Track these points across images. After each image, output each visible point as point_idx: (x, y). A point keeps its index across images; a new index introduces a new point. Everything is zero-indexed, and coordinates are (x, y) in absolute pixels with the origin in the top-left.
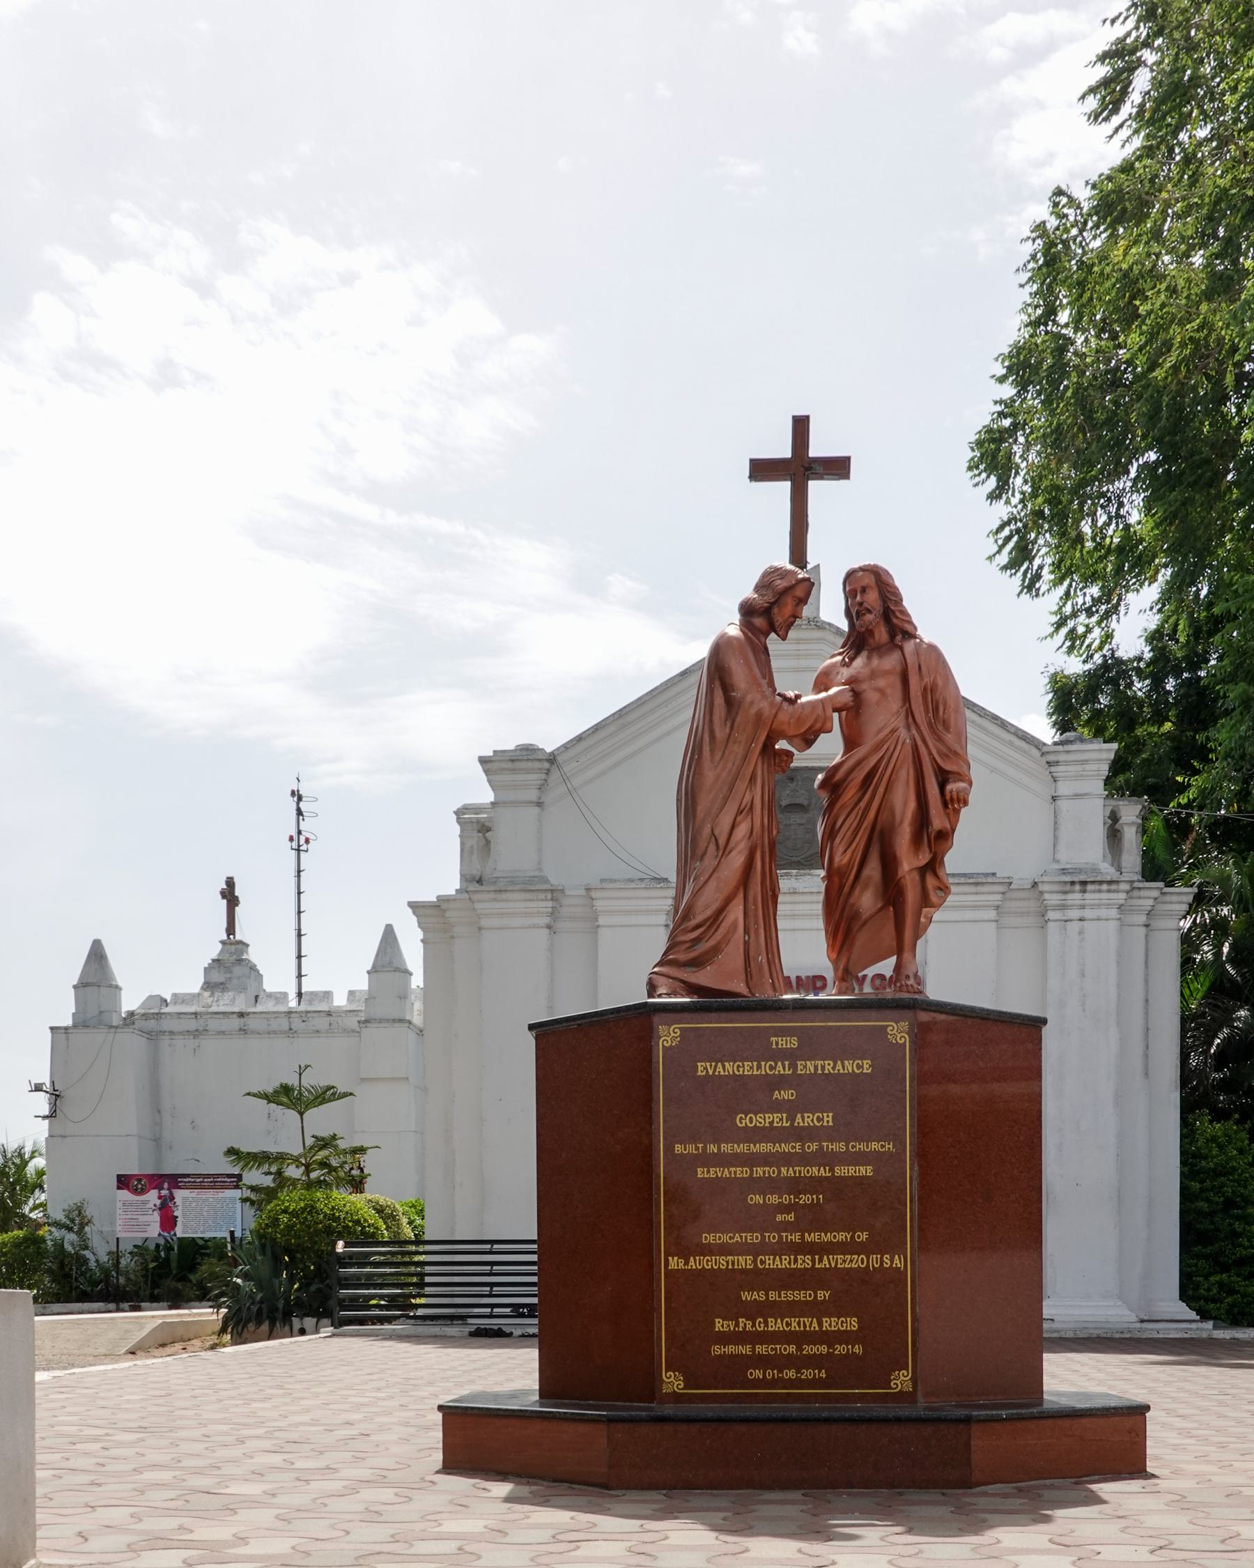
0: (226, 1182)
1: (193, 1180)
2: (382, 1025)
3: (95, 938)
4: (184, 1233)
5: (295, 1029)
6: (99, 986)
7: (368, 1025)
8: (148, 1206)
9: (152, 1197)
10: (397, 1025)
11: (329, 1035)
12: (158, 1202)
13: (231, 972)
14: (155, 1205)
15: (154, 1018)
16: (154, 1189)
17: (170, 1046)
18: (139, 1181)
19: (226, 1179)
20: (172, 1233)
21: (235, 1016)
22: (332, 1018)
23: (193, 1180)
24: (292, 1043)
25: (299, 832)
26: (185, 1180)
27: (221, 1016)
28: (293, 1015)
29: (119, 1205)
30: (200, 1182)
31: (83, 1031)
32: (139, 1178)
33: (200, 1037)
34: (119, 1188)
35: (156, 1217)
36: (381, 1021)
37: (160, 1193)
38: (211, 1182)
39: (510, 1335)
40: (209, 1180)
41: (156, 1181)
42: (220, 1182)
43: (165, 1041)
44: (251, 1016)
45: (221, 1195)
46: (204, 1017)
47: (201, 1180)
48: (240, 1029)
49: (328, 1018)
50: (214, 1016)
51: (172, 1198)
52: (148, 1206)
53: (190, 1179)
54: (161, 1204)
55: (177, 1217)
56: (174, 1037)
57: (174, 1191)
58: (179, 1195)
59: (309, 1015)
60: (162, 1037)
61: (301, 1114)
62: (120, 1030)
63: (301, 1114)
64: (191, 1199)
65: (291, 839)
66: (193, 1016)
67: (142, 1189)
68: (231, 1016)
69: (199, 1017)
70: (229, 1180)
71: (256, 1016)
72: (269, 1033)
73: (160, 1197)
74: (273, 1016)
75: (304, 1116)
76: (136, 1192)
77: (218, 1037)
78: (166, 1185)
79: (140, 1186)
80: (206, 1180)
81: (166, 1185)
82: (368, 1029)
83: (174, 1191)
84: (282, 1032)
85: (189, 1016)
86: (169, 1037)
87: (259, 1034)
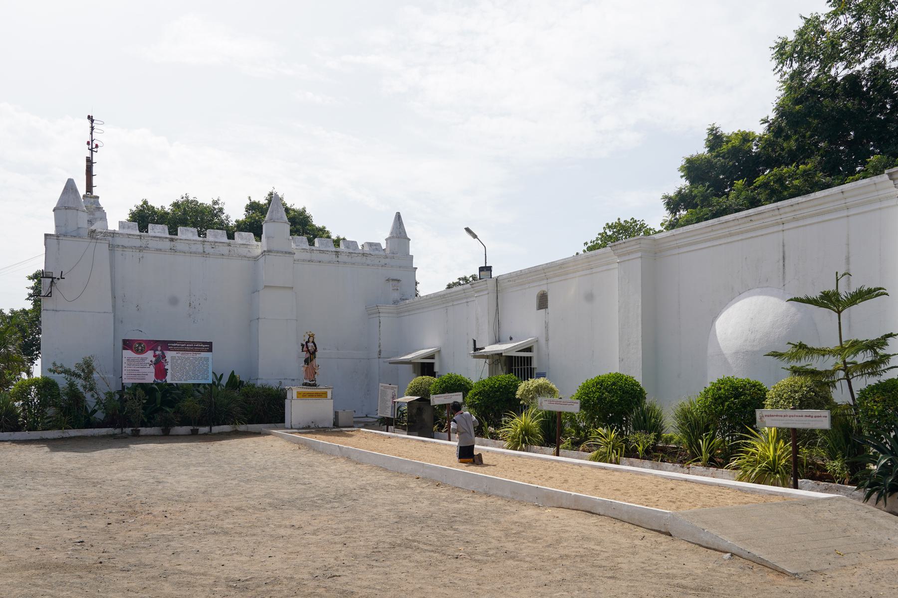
0: (202, 347)
1: (179, 345)
2: (278, 254)
3: (69, 178)
4: (172, 380)
5: (207, 252)
6: (77, 210)
7: (270, 254)
8: (146, 362)
9: (149, 356)
10: (287, 255)
11: (230, 258)
12: (154, 359)
13: (93, 215)
14: (151, 361)
15: (110, 236)
16: (150, 350)
17: (122, 255)
18: (140, 344)
19: (202, 345)
20: (164, 380)
21: (168, 240)
22: (231, 248)
23: (179, 345)
24: (206, 260)
25: (92, 141)
26: (173, 345)
27: (158, 239)
28: (206, 243)
29: (125, 360)
30: (184, 347)
31: (71, 239)
32: (140, 342)
33: (144, 251)
34: (124, 349)
35: (152, 369)
36: (278, 252)
37: (154, 353)
38: (191, 347)
39: (661, 477)
40: (190, 345)
41: (152, 345)
42: (198, 347)
43: (118, 253)
44: (178, 241)
45: (198, 356)
46: (146, 238)
47: (185, 345)
48: (171, 249)
49: (228, 248)
50: (153, 239)
51: (164, 357)
52: (146, 362)
53: (177, 344)
54: (156, 360)
55: (167, 369)
56: (126, 250)
57: (165, 352)
58: (169, 355)
59: (216, 244)
60: (117, 249)
61: (839, 313)
62: (100, 241)
63: (839, 313)
64: (177, 358)
65: (88, 143)
66: (139, 237)
67: (142, 350)
68: (164, 240)
69: (142, 238)
70: (204, 346)
71: (182, 241)
72: (191, 253)
73: (155, 356)
74: (193, 242)
75: (841, 314)
76: (137, 351)
77: (156, 252)
78: (159, 348)
79: (140, 348)
80: (187, 345)
81: (159, 348)
82: (270, 256)
83: (165, 352)
84: (199, 253)
85: (136, 237)
86: (121, 249)
87: (185, 253)
